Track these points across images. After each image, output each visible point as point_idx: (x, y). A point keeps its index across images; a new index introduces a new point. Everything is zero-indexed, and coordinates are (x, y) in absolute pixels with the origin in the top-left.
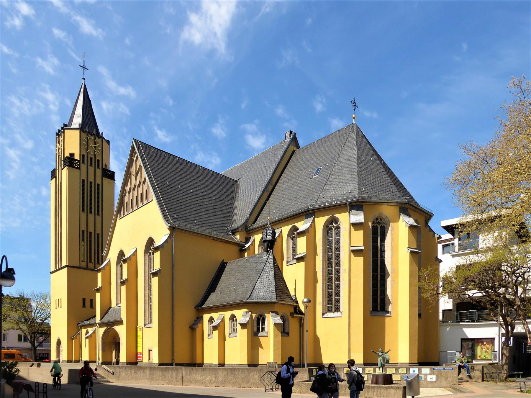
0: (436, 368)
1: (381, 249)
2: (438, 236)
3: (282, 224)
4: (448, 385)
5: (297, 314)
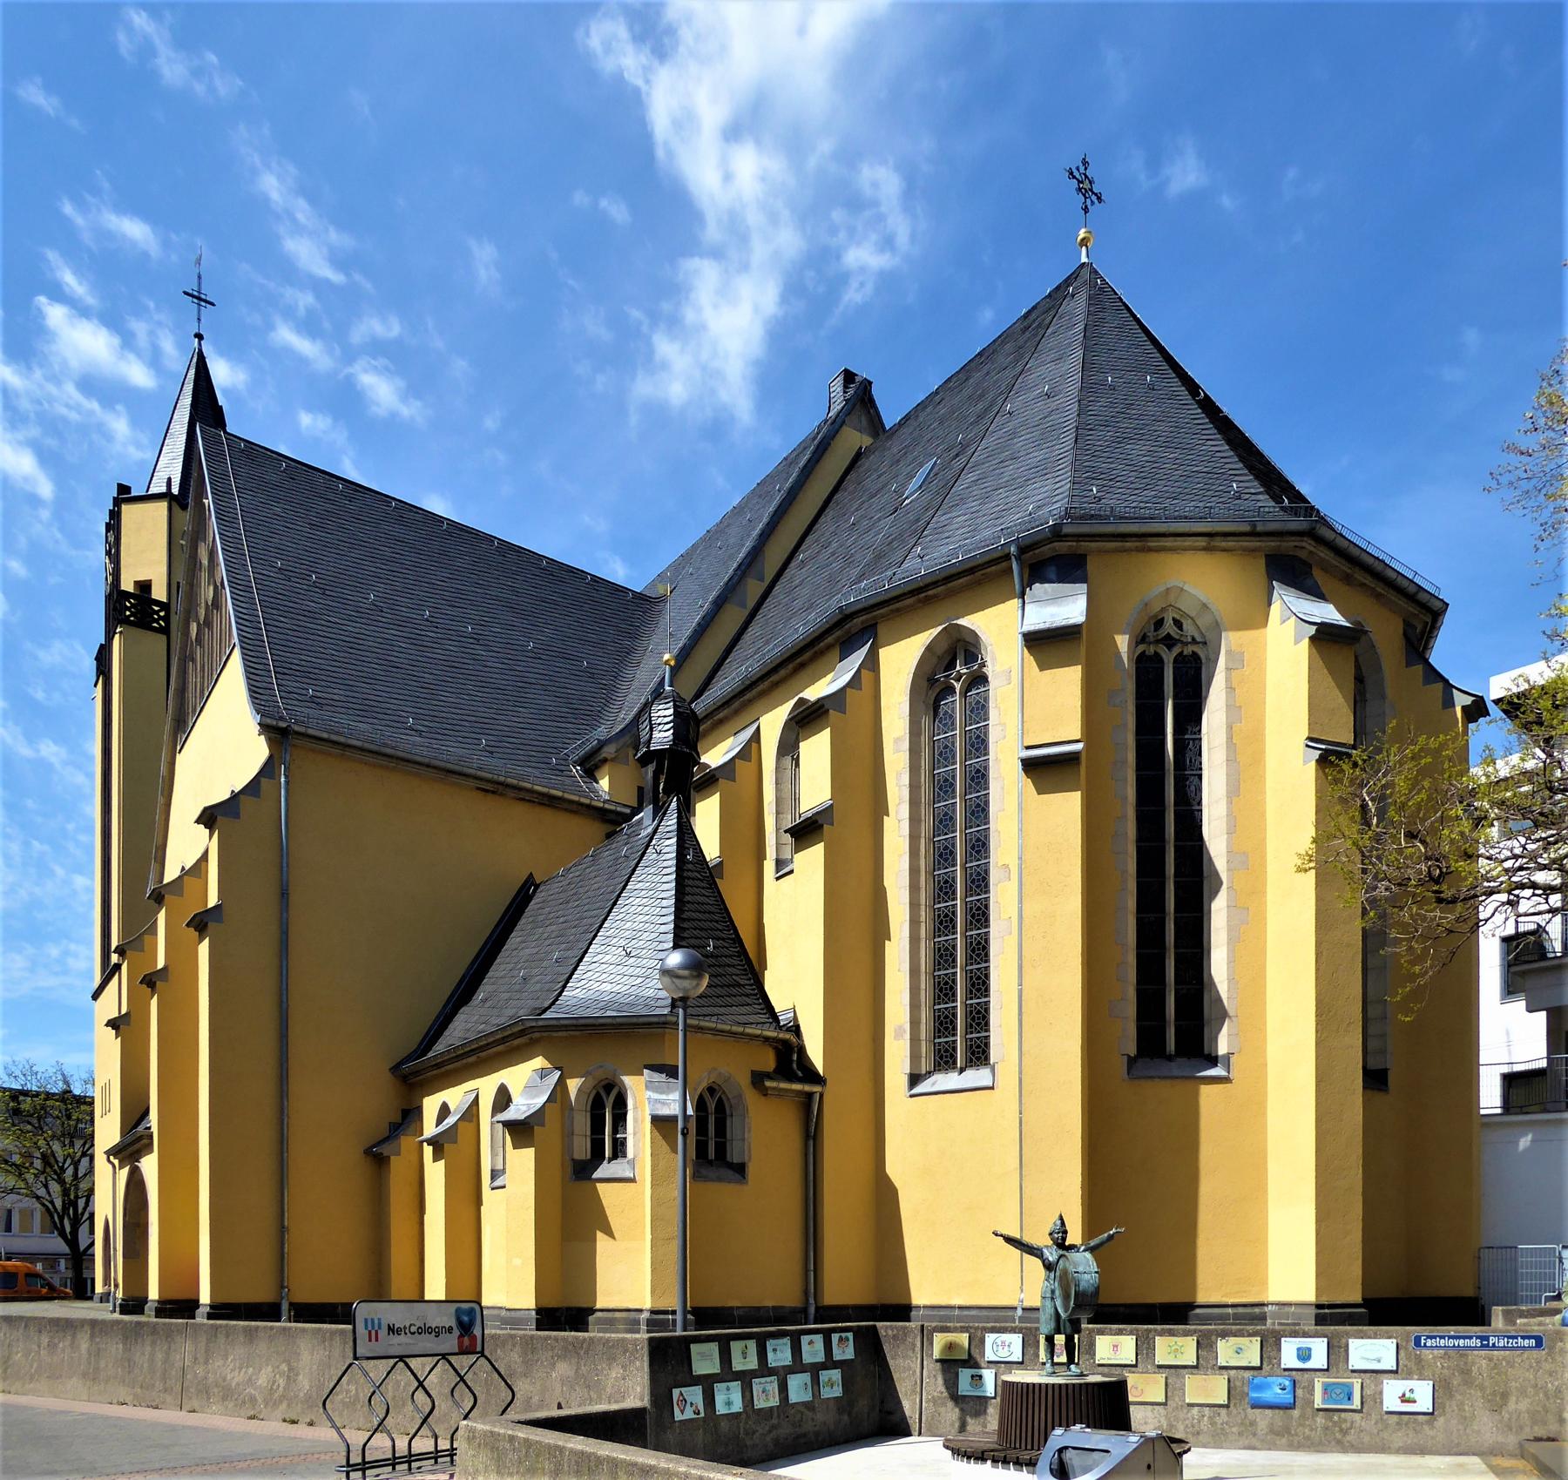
0: (1440, 1340)
2: (1468, 700)
3: (759, 705)
4: (1512, 1440)
5: (792, 1078)
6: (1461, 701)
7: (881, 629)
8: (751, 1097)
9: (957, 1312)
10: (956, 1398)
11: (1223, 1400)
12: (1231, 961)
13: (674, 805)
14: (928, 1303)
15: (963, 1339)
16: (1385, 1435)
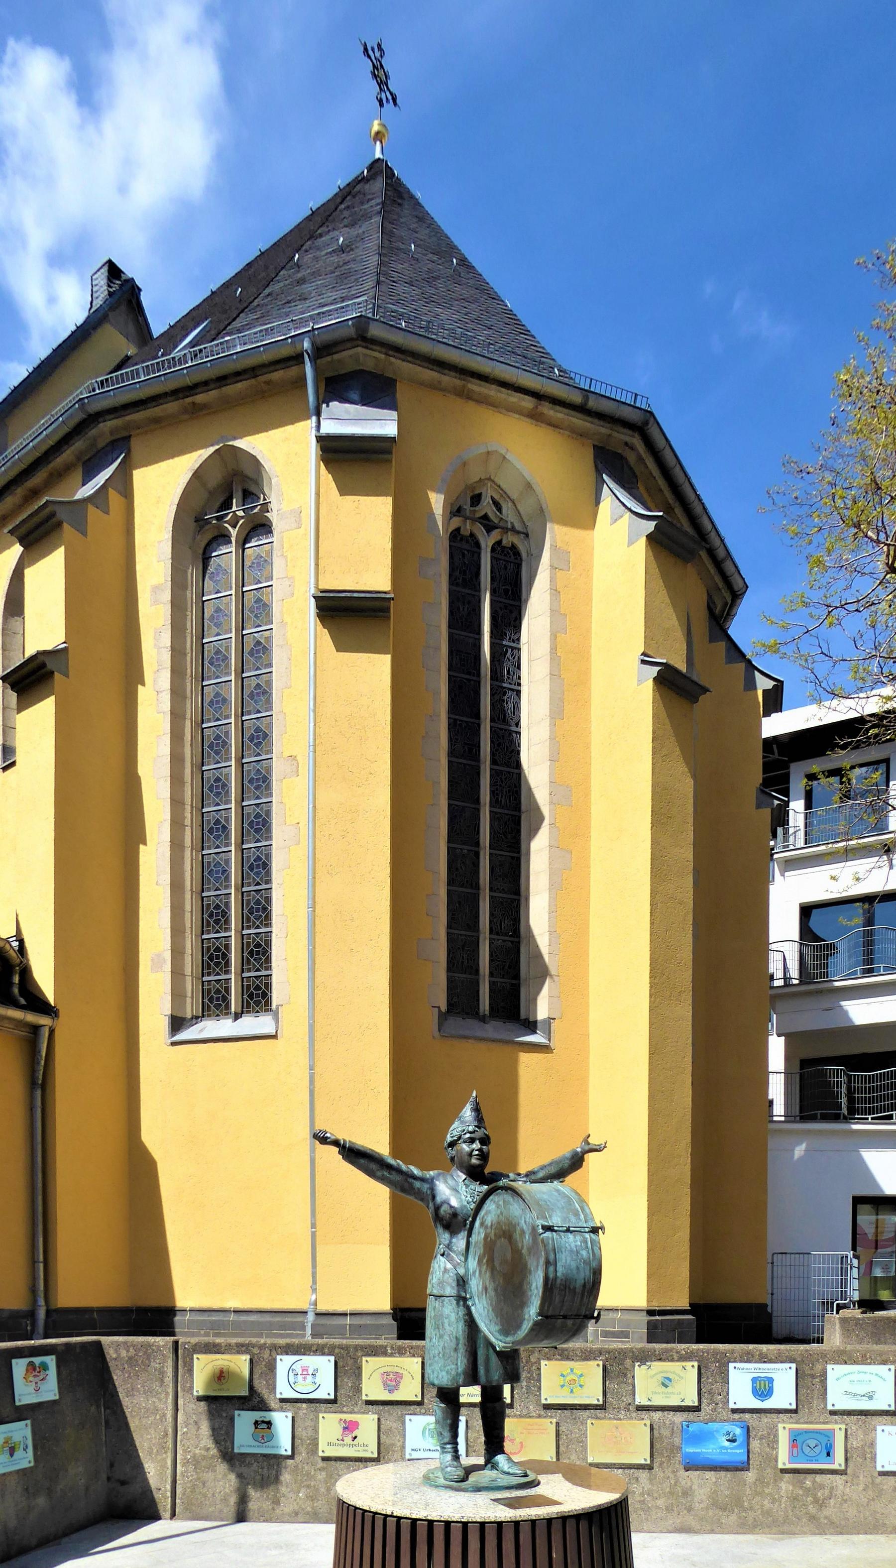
1: (496, 675)
2: (770, 684)
6: (763, 684)
7: (136, 444)
9: (232, 1317)
10: (230, 1457)
11: (643, 1457)
12: (553, 911)
15: (241, 1364)
16: (878, 1506)
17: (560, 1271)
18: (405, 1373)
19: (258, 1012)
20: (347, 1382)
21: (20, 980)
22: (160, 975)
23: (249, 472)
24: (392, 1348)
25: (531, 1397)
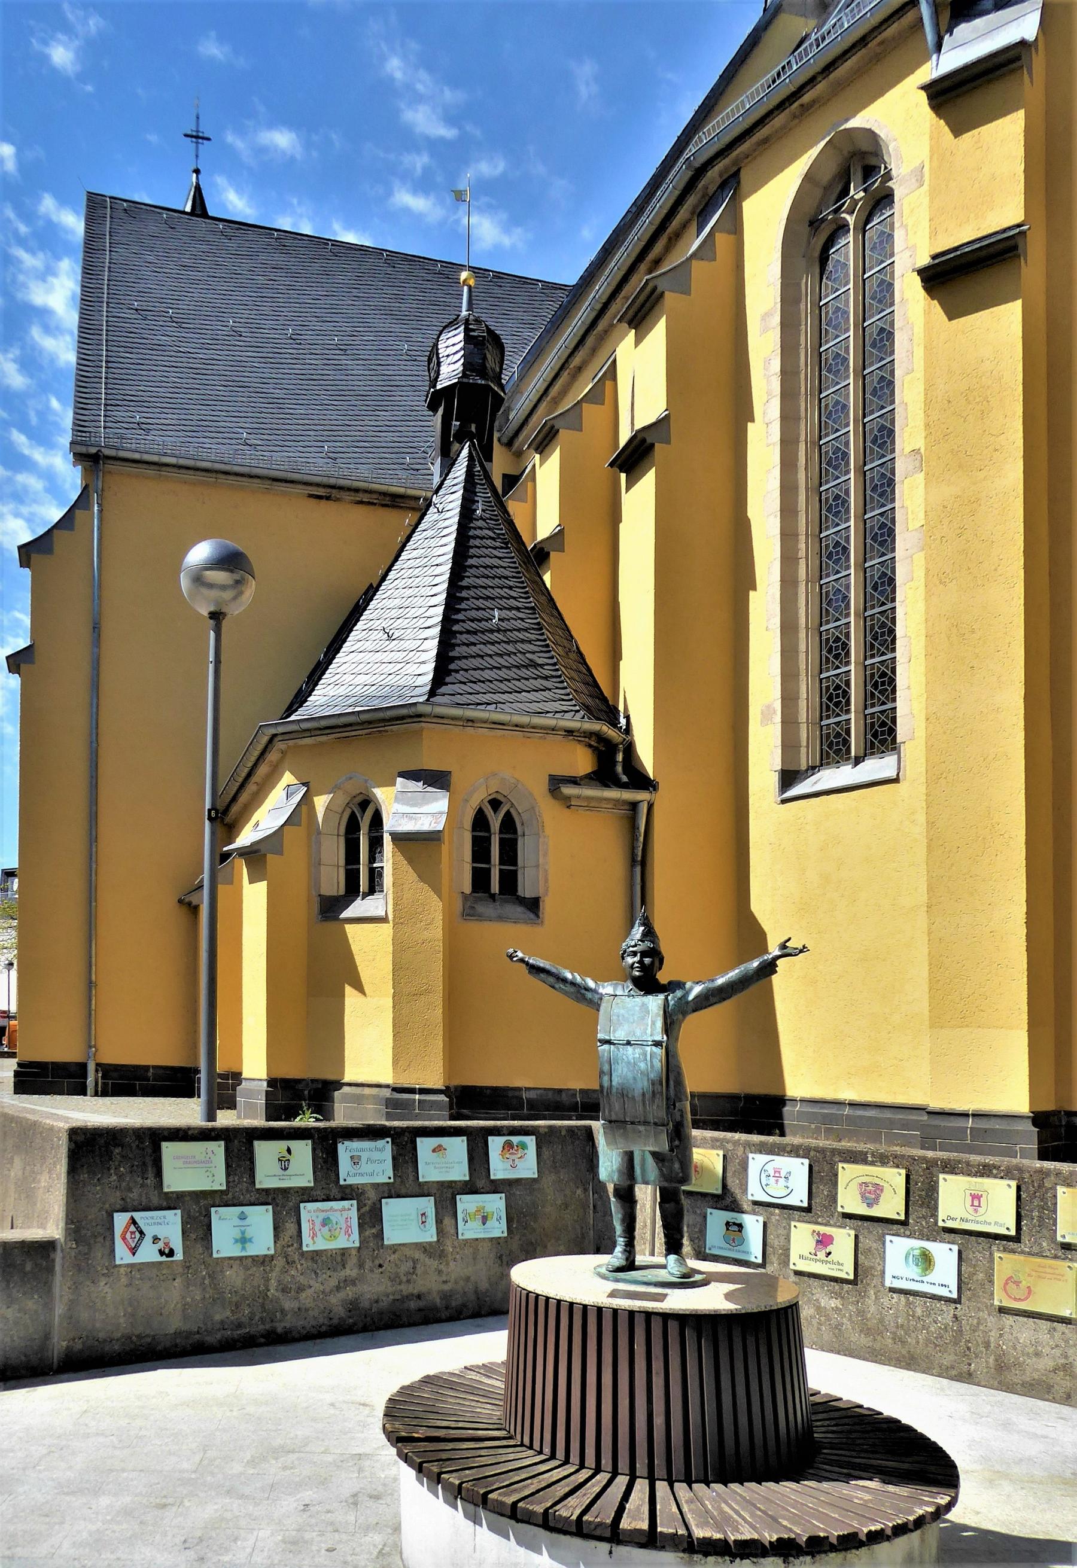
8: (549, 811)
9: (847, 1111)
13: (465, 452)
14: (808, 1094)
17: (616, 1081)
18: (886, 1185)
19: (883, 752)
20: (823, 1190)
21: (624, 758)
22: (770, 727)
23: (865, 146)
24: (873, 1155)
25: (1045, 1231)
